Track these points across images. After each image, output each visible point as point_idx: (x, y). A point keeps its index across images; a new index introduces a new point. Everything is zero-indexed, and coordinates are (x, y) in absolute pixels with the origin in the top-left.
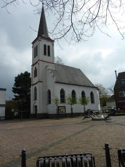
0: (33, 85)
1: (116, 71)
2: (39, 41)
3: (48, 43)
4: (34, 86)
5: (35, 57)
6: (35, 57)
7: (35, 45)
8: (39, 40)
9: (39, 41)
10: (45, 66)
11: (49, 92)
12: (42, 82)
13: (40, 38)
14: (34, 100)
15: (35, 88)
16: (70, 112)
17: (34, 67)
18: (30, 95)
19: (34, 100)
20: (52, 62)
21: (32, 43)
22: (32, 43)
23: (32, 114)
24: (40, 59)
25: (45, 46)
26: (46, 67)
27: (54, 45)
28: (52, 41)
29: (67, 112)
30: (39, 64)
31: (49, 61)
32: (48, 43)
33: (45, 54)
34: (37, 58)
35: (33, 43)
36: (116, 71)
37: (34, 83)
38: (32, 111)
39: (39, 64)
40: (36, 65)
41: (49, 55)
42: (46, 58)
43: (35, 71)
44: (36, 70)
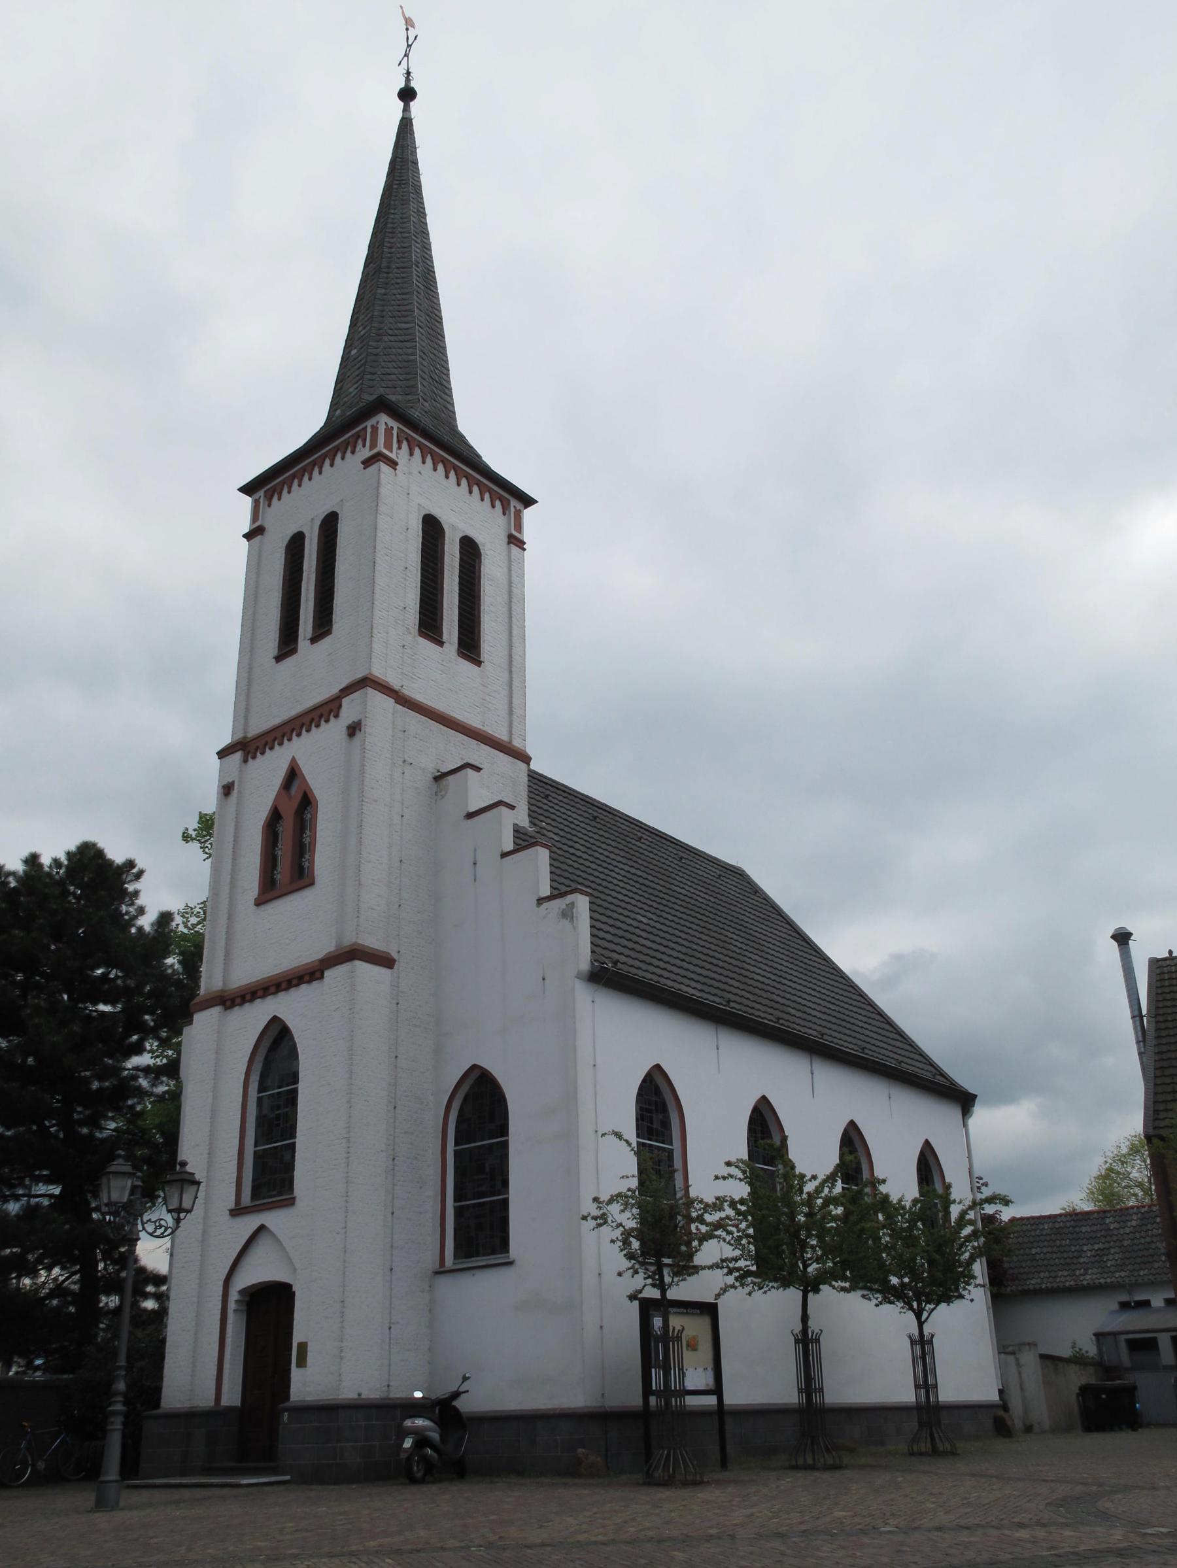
0: (231, 1000)
1: (1122, 938)
2: (367, 463)
3: (466, 514)
4: (250, 1021)
5: (288, 643)
6: (288, 643)
7: (300, 510)
8: (364, 453)
9: (367, 463)
10: (431, 763)
11: (480, 1110)
12: (385, 961)
13: (389, 430)
14: (237, 1211)
15: (277, 1045)
16: (906, 1395)
17: (268, 773)
18: (472, 1087)
19: (237, 1211)
20: (501, 734)
21: (247, 489)
22: (247, 489)
23: (189, 1417)
24: (378, 672)
25: (432, 528)
26: (439, 778)
27: (520, 544)
28: (511, 497)
29: (734, 1396)
30: (353, 730)
31: (474, 722)
32: (466, 514)
33: (430, 625)
34: (317, 670)
35: (266, 487)
36: (1122, 938)
37: (245, 974)
38: (198, 1365)
39: (353, 730)
40: (316, 753)
41: (470, 646)
42: (434, 672)
43: (275, 817)
44: (307, 802)
